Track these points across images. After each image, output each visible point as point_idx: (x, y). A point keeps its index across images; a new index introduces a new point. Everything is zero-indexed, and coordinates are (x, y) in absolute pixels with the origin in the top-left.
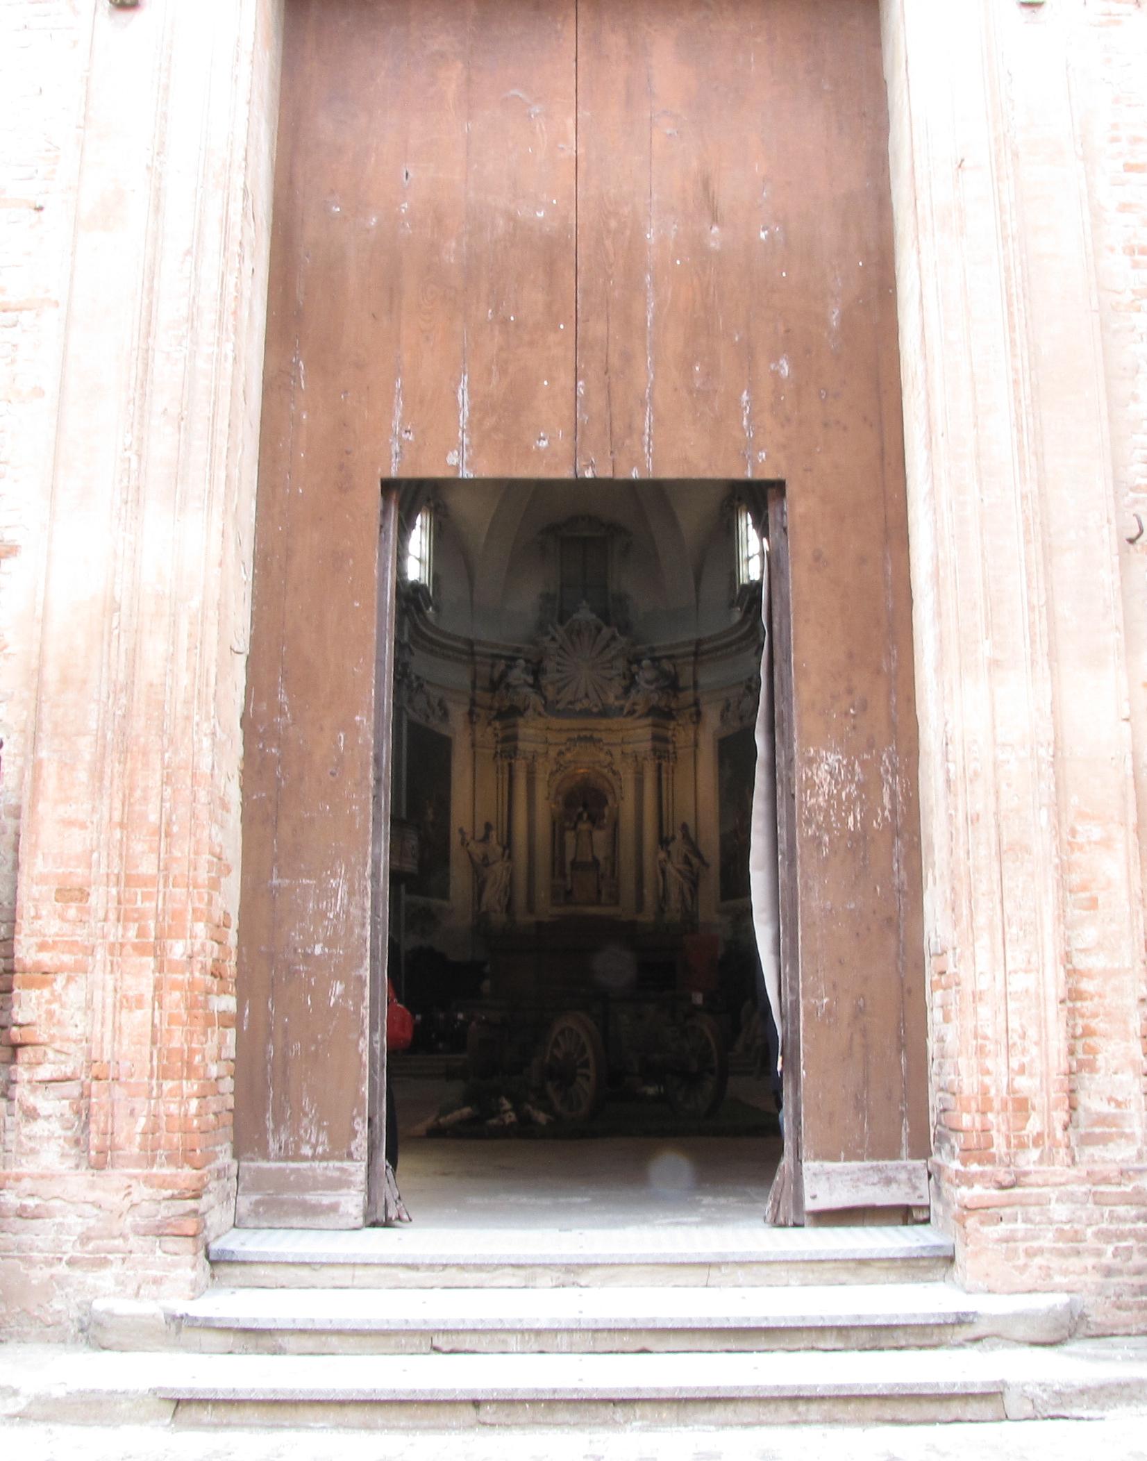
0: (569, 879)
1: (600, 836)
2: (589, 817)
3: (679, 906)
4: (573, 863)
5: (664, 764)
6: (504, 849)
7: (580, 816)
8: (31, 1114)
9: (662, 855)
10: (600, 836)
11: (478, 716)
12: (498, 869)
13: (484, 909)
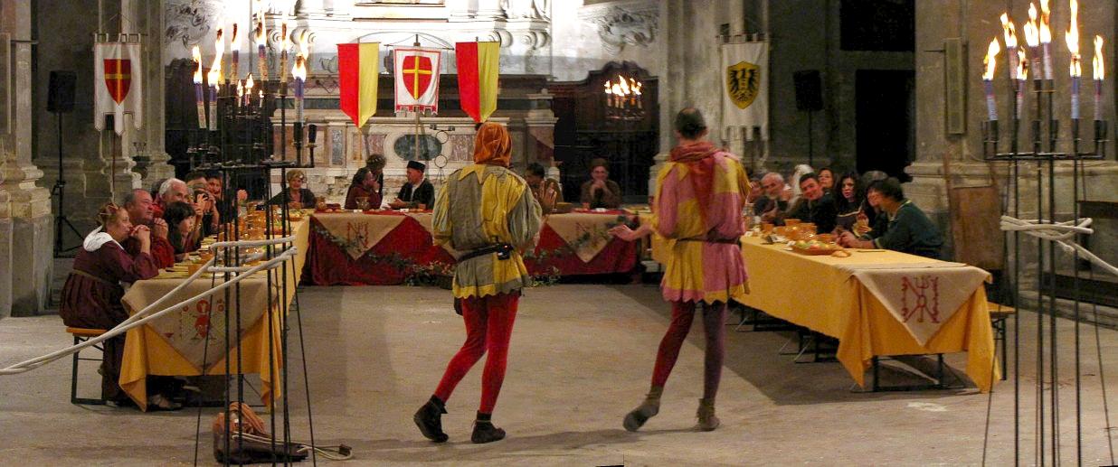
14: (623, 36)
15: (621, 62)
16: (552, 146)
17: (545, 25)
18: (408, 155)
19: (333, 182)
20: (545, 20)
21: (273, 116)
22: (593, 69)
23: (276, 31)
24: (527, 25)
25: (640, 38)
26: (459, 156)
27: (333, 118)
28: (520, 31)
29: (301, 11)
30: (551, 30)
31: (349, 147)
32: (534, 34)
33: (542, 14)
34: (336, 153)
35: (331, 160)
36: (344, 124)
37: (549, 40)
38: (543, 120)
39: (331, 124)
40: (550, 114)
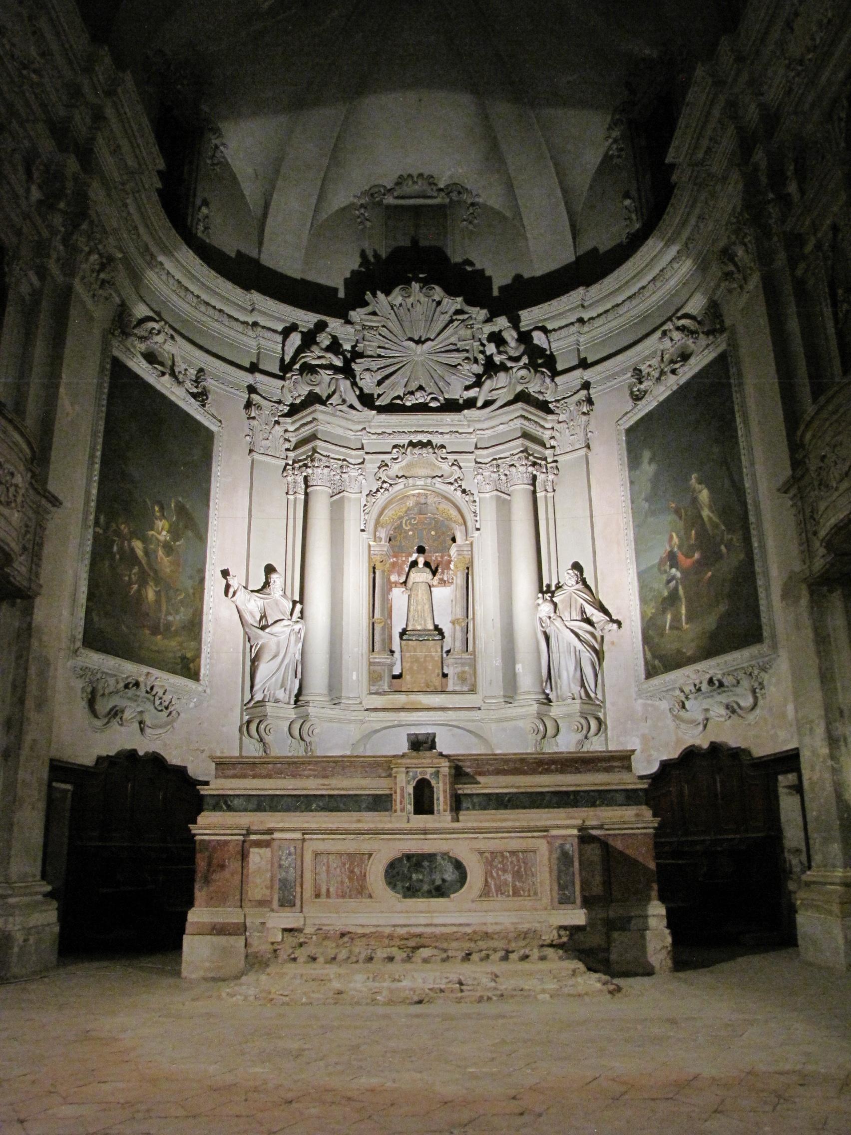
0: (397, 655)
1: (445, 596)
2: (427, 564)
3: (576, 689)
4: (403, 633)
5: (541, 477)
6: (294, 603)
7: (414, 564)
8: (444, 881)
9: (546, 608)
10: (445, 596)
11: (259, 407)
12: (281, 636)
13: (258, 697)
14: (707, 710)
15: (705, 745)
16: (652, 865)
17: (598, 708)
18: (408, 889)
19: (279, 938)
20: (598, 702)
21: (195, 823)
22: (665, 758)
23: (268, 722)
24: (577, 706)
25: (732, 709)
26: (499, 889)
27: (280, 825)
28: (568, 716)
29: (301, 698)
30: (605, 714)
31: (308, 876)
32: (586, 718)
33: (592, 695)
34: (285, 885)
35: (276, 898)
36: (298, 835)
37: (603, 727)
38: (637, 822)
39: (276, 835)
40: (647, 813)
